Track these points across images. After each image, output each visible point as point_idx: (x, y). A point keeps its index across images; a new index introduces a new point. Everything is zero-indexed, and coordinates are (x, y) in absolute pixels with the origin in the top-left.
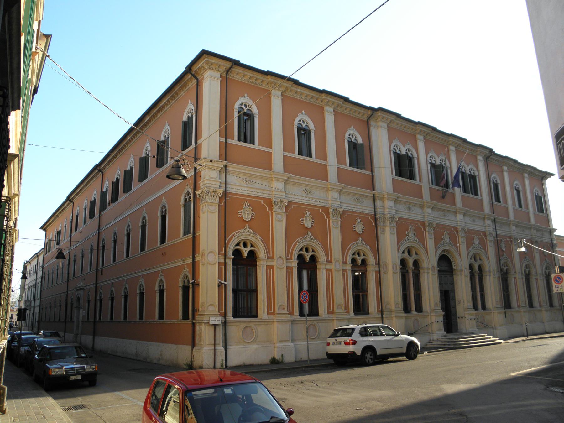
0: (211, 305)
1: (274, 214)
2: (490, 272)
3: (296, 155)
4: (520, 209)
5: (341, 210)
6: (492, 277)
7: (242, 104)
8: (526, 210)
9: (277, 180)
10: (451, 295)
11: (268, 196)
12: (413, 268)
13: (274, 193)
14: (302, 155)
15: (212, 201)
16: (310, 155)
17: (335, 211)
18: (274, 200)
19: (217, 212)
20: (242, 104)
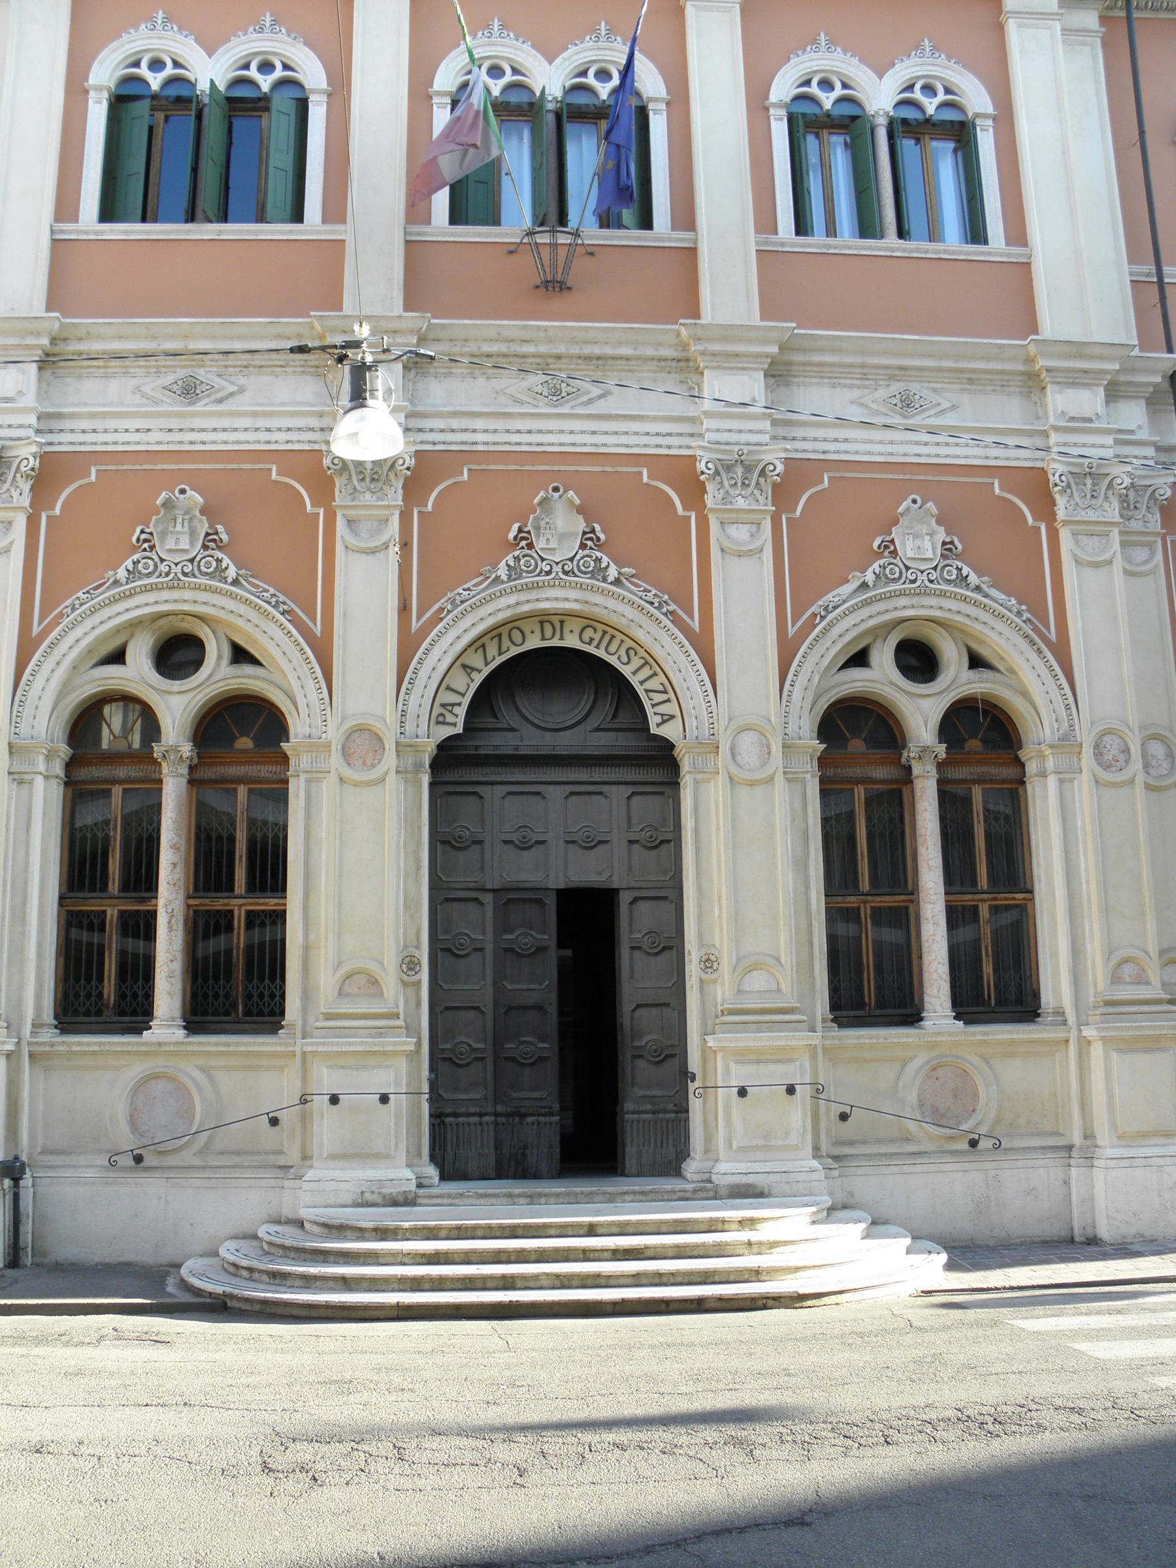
0: (638, 1006)
1: (1065, 535)
2: (1067, 743)
3: (847, 240)
4: (974, 251)
5: (774, 457)
6: (1083, 787)
7: (910, 88)
8: (680, 239)
9: (730, 361)
10: (634, 924)
11: (676, 447)
12: (941, 750)
13: (707, 424)
14: (608, 227)
15: (1092, 515)
16: (646, 222)
17: (741, 467)
18: (1057, 469)
19: (768, 554)
20: (910, 88)
